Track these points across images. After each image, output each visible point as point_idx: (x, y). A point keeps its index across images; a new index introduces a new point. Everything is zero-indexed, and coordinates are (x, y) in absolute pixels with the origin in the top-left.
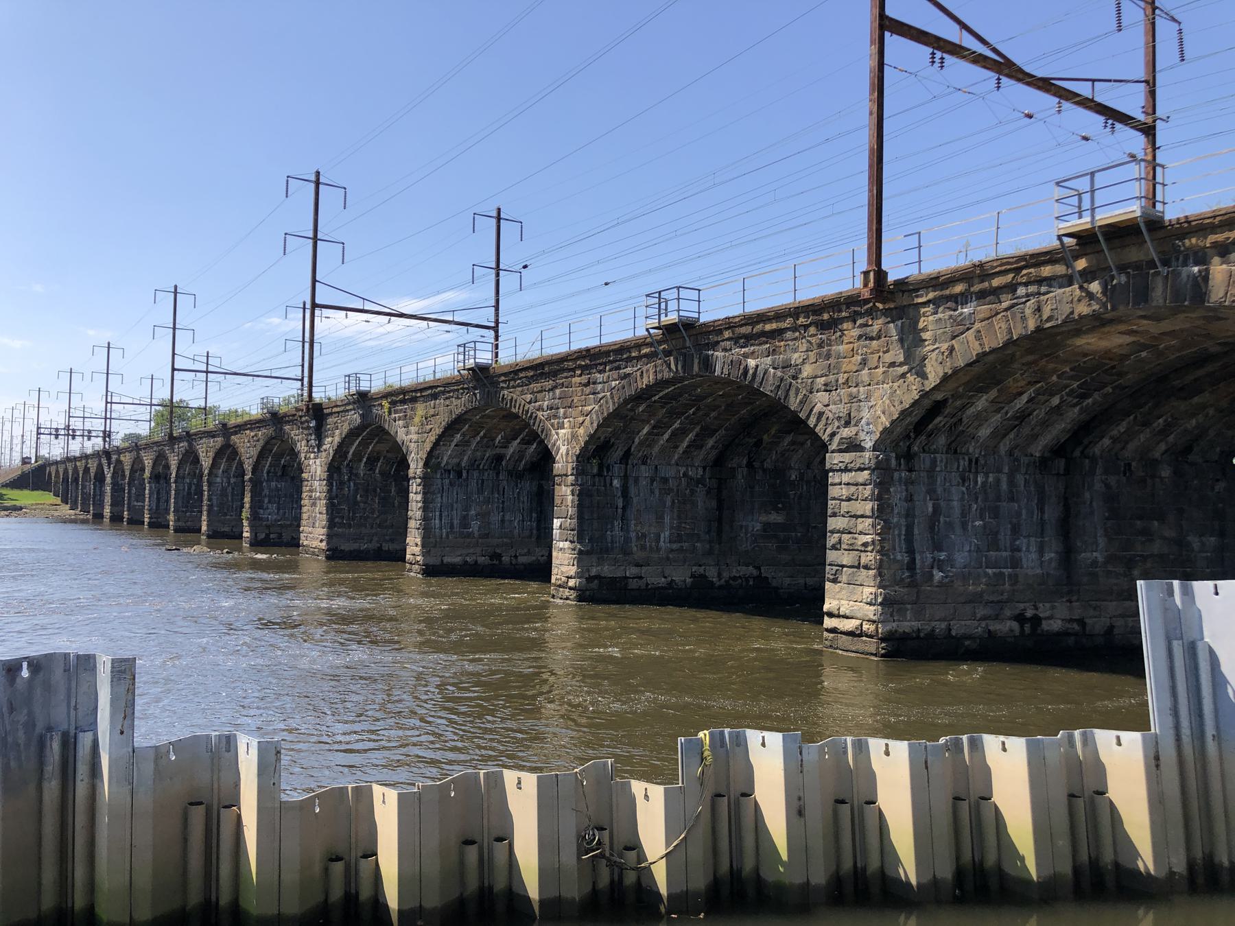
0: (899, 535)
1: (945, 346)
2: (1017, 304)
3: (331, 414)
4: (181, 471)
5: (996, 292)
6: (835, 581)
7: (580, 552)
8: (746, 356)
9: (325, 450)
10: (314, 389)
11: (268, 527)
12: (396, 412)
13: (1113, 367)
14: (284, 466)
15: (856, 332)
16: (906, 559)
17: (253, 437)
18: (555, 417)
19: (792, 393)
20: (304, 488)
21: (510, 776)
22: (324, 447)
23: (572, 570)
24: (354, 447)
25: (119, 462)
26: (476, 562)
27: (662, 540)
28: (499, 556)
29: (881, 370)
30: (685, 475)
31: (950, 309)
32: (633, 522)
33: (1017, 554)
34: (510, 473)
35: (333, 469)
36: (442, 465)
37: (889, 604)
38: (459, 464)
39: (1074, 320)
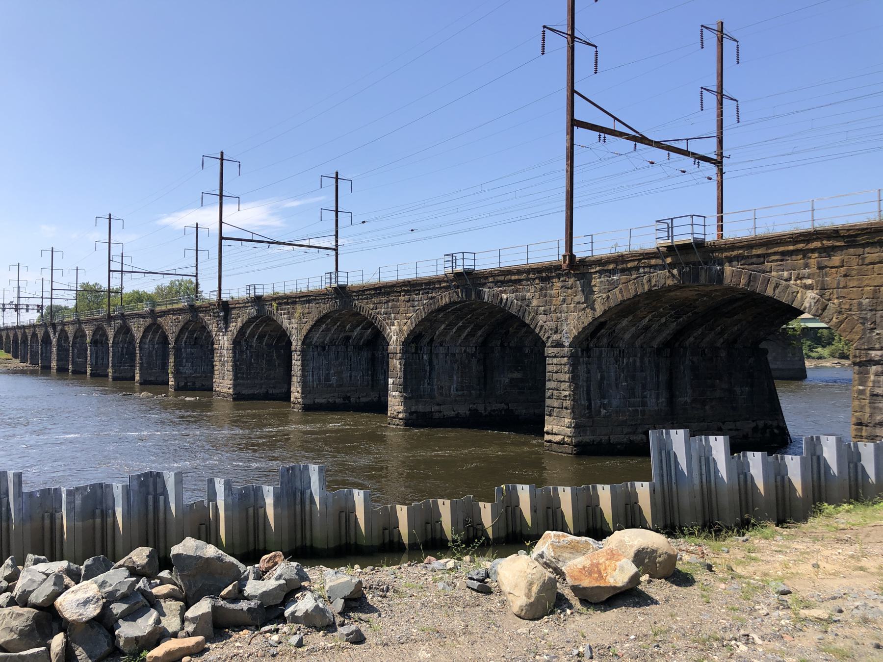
0: (583, 391)
1: (605, 295)
2: (640, 277)
3: (235, 308)
4: (116, 339)
5: (629, 270)
6: (550, 415)
7: (406, 398)
8: (501, 292)
9: (231, 331)
10: (222, 292)
11: (186, 378)
12: (282, 310)
13: (691, 304)
14: (196, 338)
15: (560, 284)
16: (587, 404)
17: (175, 320)
18: (389, 319)
19: (527, 314)
20: (215, 355)
21: (440, 501)
22: (230, 329)
23: (401, 408)
24: (250, 329)
25: (63, 331)
26: (335, 402)
27: (452, 389)
28: (349, 398)
29: (572, 305)
30: (465, 351)
31: (607, 276)
32: (436, 380)
33: (645, 399)
34: (355, 347)
35: (236, 343)
36: (313, 343)
37: (578, 428)
38: (323, 342)
39: (666, 287)
